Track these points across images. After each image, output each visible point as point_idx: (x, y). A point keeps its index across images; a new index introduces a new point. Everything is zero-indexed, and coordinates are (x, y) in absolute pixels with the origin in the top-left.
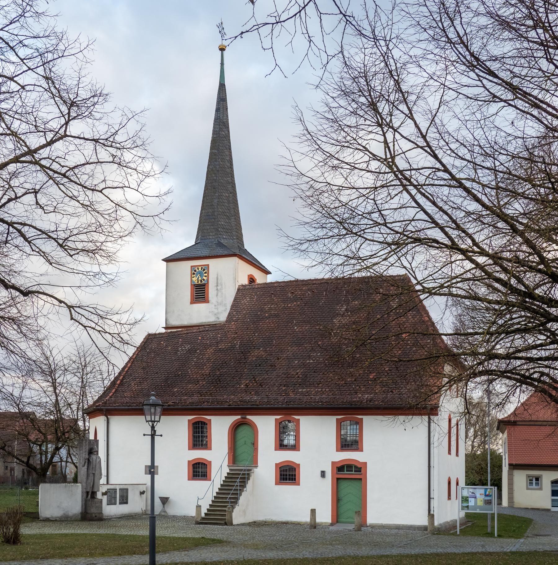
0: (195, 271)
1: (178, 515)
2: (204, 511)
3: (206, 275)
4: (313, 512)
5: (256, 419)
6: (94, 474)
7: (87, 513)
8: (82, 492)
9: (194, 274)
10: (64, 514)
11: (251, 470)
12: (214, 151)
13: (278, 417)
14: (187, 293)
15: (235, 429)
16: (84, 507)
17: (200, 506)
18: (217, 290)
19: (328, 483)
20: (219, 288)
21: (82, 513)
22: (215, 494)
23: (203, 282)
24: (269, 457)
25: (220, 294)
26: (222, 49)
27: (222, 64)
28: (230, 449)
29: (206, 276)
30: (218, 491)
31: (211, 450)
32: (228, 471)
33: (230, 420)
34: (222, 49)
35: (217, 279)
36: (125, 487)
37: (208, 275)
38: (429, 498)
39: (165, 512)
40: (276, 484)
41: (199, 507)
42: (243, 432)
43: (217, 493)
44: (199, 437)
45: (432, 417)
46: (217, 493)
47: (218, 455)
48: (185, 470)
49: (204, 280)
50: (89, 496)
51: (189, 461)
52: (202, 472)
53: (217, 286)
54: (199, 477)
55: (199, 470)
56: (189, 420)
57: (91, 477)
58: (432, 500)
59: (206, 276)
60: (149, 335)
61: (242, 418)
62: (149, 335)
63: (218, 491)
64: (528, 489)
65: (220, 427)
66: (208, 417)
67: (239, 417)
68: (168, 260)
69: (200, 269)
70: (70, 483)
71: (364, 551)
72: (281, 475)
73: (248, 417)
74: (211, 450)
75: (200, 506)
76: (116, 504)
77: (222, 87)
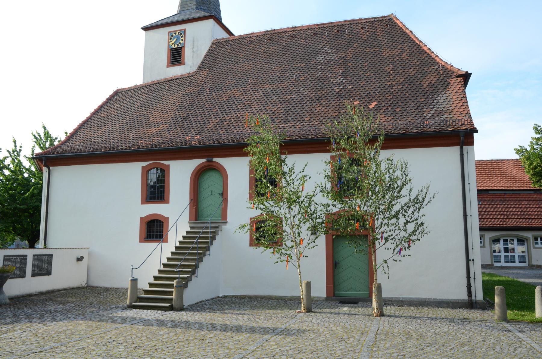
0: (172, 36)
2: (144, 284)
3: (183, 38)
4: (308, 285)
9: (171, 39)
11: (217, 227)
14: (164, 56)
15: (198, 177)
17: (136, 280)
18: (193, 51)
20: (194, 50)
23: (180, 46)
24: (241, 209)
28: (191, 200)
29: (182, 40)
31: (169, 203)
37: (185, 38)
38: (468, 260)
40: (251, 245)
41: (134, 281)
42: (211, 181)
43: (168, 259)
44: (156, 192)
45: (465, 147)
46: (168, 259)
48: (135, 230)
49: (180, 43)
51: (141, 218)
52: (157, 232)
53: (193, 48)
54: (153, 238)
55: (154, 230)
56: (143, 167)
58: (471, 263)
59: (182, 40)
61: (208, 161)
63: (170, 256)
65: (180, 174)
66: (166, 163)
67: (204, 160)
68: (146, 29)
69: (177, 34)
71: (327, 310)
72: (467, 102)
73: (215, 160)
74: (169, 203)
75: (136, 280)
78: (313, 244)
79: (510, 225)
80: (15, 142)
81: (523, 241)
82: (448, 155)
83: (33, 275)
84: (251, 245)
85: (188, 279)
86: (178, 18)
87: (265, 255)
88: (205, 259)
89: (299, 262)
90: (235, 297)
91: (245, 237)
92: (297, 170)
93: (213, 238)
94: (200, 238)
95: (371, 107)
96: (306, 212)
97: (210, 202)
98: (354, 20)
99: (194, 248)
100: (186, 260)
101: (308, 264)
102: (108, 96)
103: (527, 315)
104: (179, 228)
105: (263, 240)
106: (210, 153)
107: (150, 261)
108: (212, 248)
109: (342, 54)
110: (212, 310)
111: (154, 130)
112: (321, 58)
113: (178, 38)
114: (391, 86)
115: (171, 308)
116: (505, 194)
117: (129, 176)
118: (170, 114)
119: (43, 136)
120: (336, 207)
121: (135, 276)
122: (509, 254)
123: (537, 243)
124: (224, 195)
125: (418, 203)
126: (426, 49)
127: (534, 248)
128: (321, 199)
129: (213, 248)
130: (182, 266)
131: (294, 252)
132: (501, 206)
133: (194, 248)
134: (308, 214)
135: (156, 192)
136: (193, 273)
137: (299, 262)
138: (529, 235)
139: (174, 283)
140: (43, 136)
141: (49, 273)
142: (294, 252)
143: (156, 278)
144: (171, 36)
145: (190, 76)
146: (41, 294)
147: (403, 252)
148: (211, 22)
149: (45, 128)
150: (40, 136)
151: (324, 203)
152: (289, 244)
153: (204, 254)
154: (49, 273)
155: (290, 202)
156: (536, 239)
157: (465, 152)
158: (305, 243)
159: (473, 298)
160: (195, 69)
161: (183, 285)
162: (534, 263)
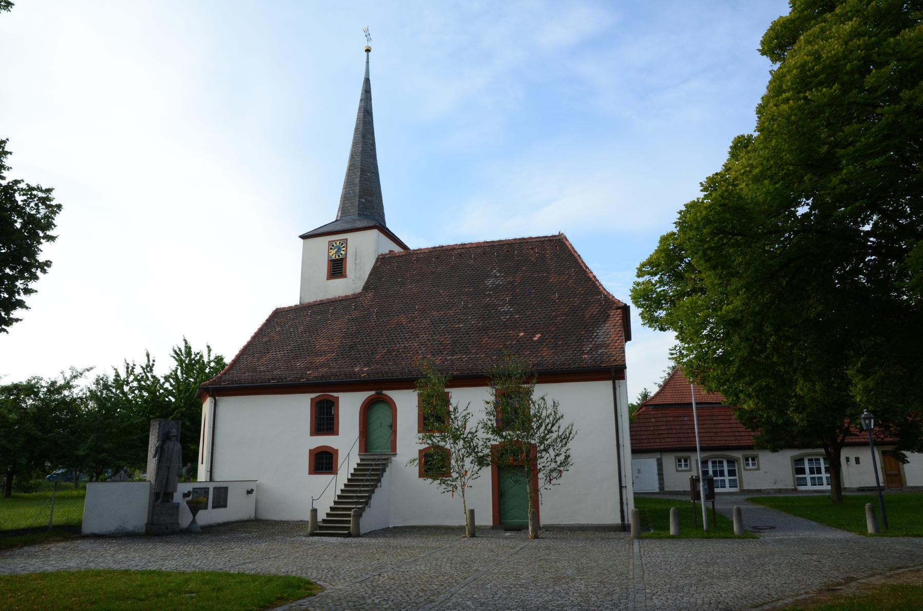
2: (321, 516)
6: (169, 468)
15: (367, 409)
22: (339, 493)
24: (409, 442)
26: (368, 51)
27: (368, 62)
28: (361, 432)
30: (343, 487)
31: (337, 434)
32: (359, 461)
34: (368, 51)
36: (224, 485)
38: (621, 487)
40: (420, 476)
41: (314, 512)
42: (380, 414)
43: (342, 491)
44: (324, 421)
45: (617, 381)
46: (342, 491)
47: (346, 443)
48: (304, 462)
50: (160, 500)
55: (323, 462)
58: (624, 490)
61: (377, 394)
62: (277, 309)
63: (343, 487)
64: (677, 471)
65: (349, 406)
67: (373, 393)
68: (304, 237)
73: (385, 392)
76: (206, 508)
77: (367, 81)
78: (476, 476)
79: (718, 444)
80: (148, 356)
81: (733, 462)
82: (603, 388)
83: (214, 507)
84: (420, 476)
85: (363, 509)
86: (338, 228)
87: (432, 486)
88: (377, 490)
89: (463, 492)
90: (405, 527)
91: (415, 470)
92: (460, 409)
93: (384, 470)
94: (373, 470)
95: (535, 339)
96: (470, 446)
97: (379, 434)
98: (524, 239)
99: (368, 480)
100: (361, 491)
101: (478, 491)
102: (267, 317)
103: (663, 533)
104: (349, 458)
105: (430, 473)
106: (379, 387)
107: (325, 492)
108: (383, 480)
109: (510, 279)
110: (385, 536)
111: (322, 359)
112: (489, 282)
113: (339, 249)
114: (557, 316)
115: (349, 535)
116: (714, 408)
117: (299, 407)
118: (337, 342)
119: (183, 352)
120: (496, 441)
121: (315, 507)
122: (816, 476)
123: (748, 464)
124: (393, 427)
125: (565, 439)
126: (591, 276)
127: (745, 470)
128: (482, 434)
129: (384, 480)
130: (357, 497)
131: (458, 483)
132: (709, 422)
133: (368, 480)
134: (472, 449)
135: (324, 421)
136: (366, 503)
137: (463, 492)
138: (739, 455)
139: (352, 513)
140: (183, 352)
141: (225, 506)
142: (458, 483)
143: (332, 509)
144: (331, 245)
145: (354, 298)
146: (219, 525)
147: (554, 481)
148: (375, 232)
149: (186, 343)
150: (180, 351)
151: (486, 440)
152: (455, 475)
153: (376, 486)
154: (225, 506)
155: (456, 438)
156: (747, 460)
157: (617, 386)
158: (469, 474)
159: (626, 522)
160: (359, 289)
161: (359, 515)
162: (746, 487)
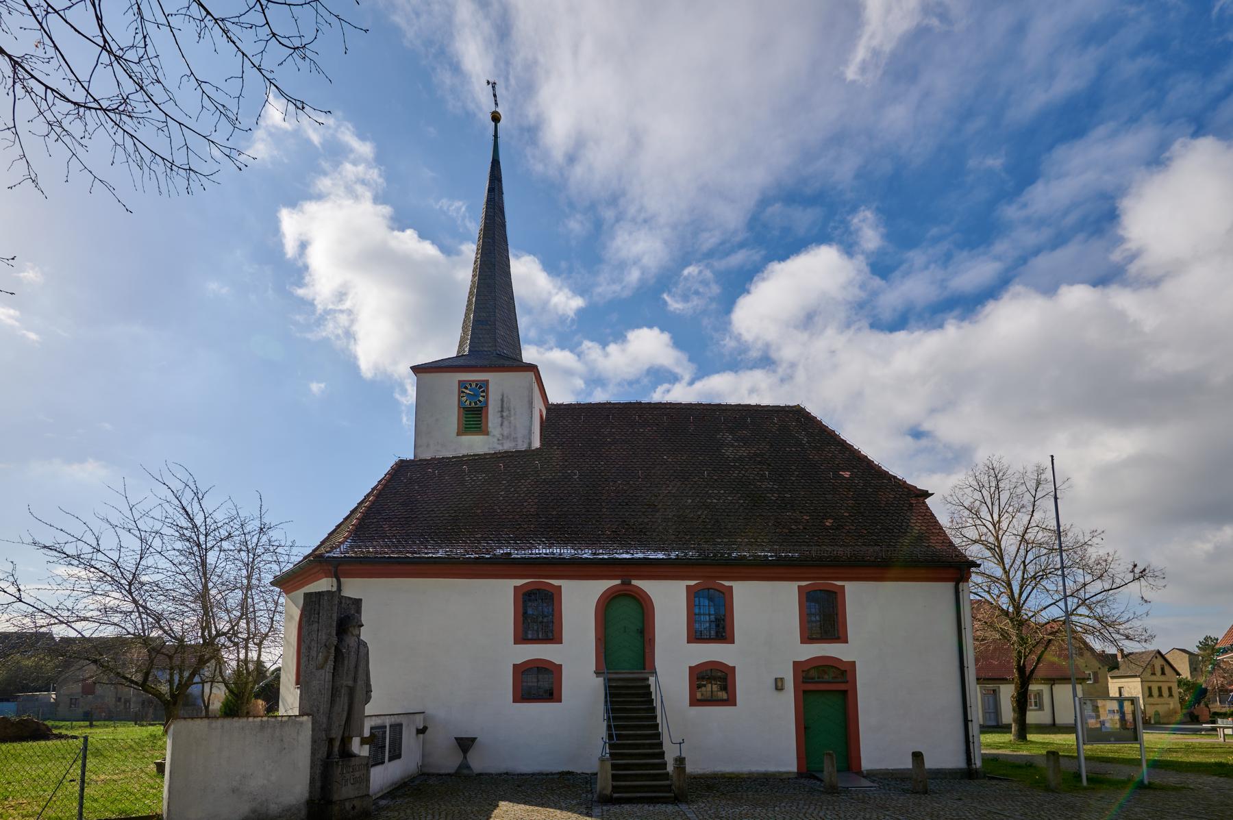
1: (492, 771)
4: (917, 756)
5: (649, 587)
7: (330, 802)
8: (314, 741)
10: (254, 811)
12: (150, 715)
13: (692, 583)
14: (452, 419)
15: (606, 605)
16: (318, 784)
19: (787, 700)
21: (310, 803)
23: (479, 405)
25: (506, 423)
33: (600, 587)
35: (502, 401)
39: (469, 767)
44: (538, 618)
56: (515, 588)
57: (343, 700)
60: (402, 461)
61: (623, 583)
66: (555, 582)
67: (618, 582)
70: (215, 717)
73: (634, 582)
77: (495, 163)
